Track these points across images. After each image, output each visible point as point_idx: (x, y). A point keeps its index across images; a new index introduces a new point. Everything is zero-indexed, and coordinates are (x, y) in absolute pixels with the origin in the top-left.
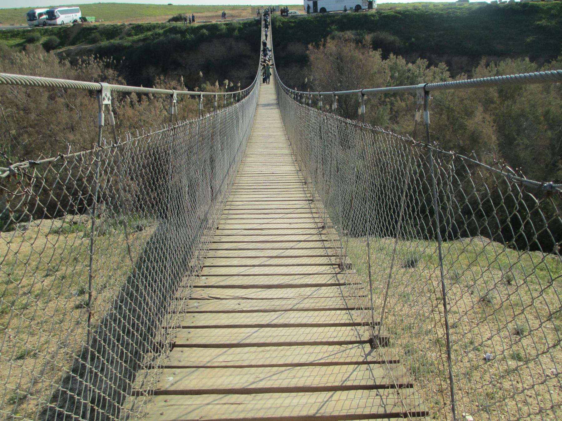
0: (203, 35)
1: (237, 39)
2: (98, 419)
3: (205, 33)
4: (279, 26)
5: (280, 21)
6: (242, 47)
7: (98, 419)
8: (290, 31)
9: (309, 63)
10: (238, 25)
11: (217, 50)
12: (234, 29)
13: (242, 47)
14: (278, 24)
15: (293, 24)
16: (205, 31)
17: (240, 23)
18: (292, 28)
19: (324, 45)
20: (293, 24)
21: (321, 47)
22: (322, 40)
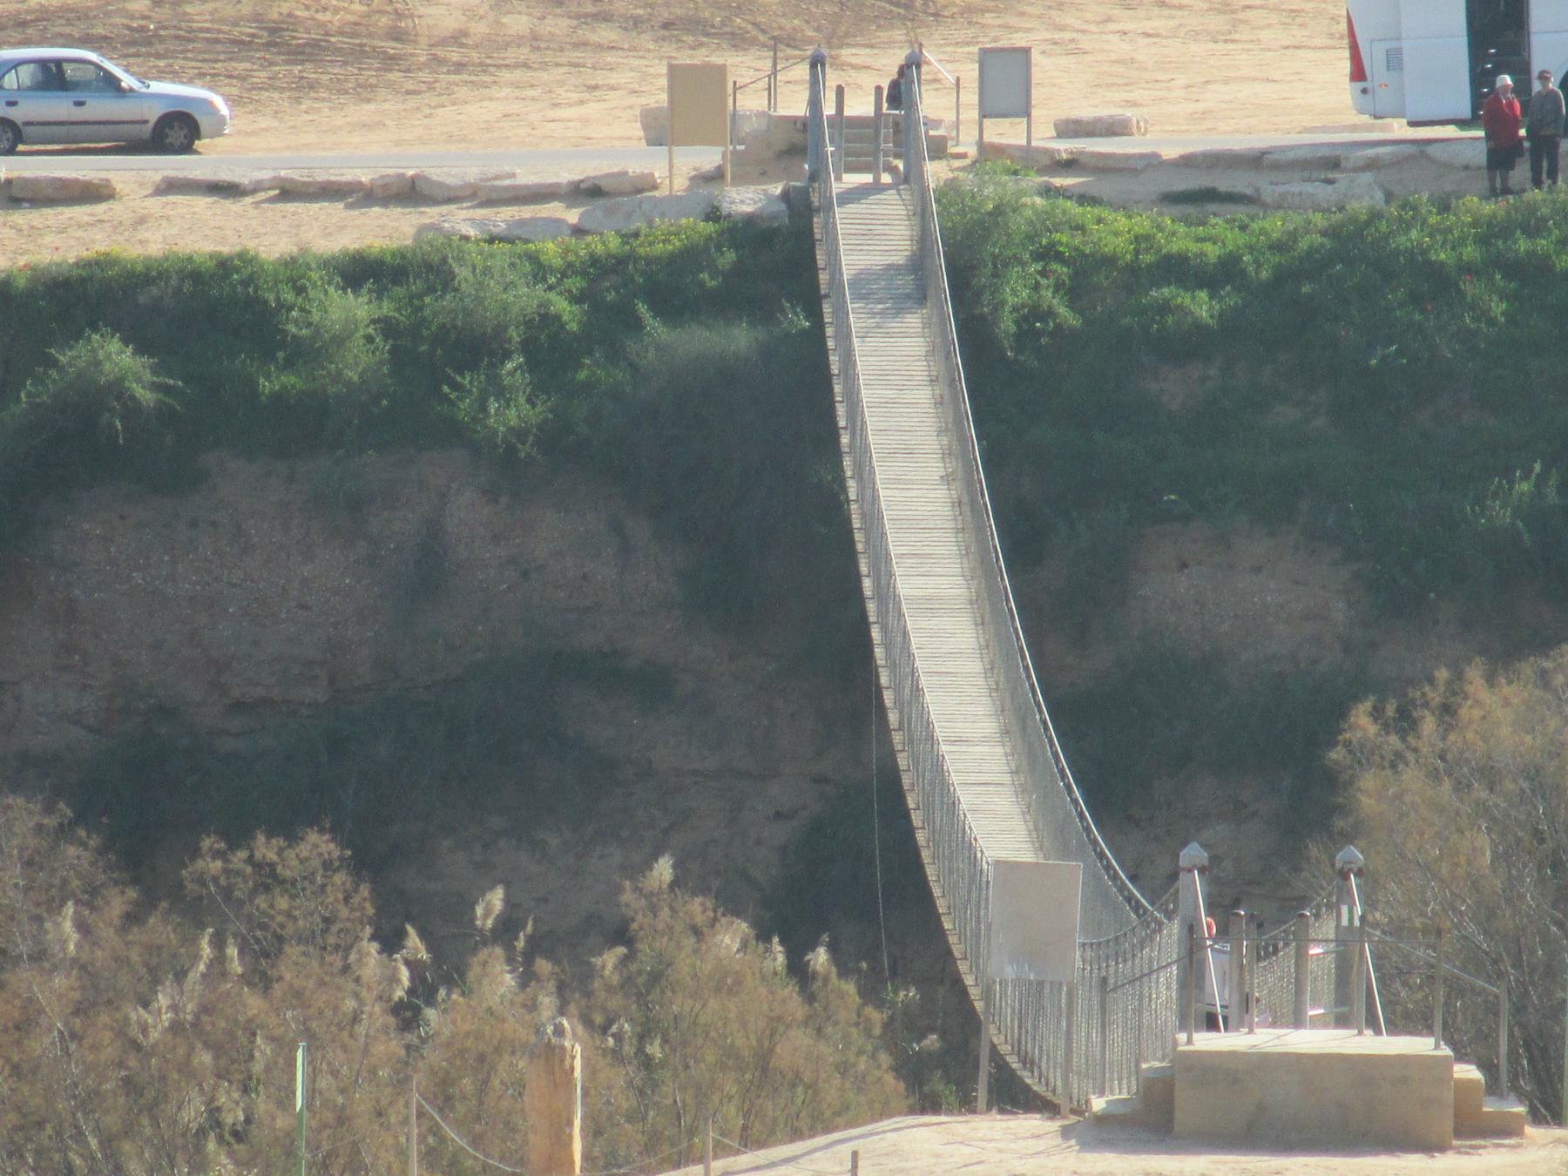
0: (92, 400)
1: (509, 470)
2: (14, 196)
3: (116, 389)
4: (1033, 314)
5: (1048, 254)
6: (576, 565)
7: (14, 196)
8: (1174, 389)
9: (1339, 823)
10: (526, 297)
11: (250, 589)
12: (473, 347)
13: (576, 565)
14: (1015, 292)
15: (1201, 306)
16: (117, 357)
17: (539, 271)
18: (1192, 345)
19: (1447, 711)
20: (1201, 306)
21: (1429, 725)
22: (1442, 674)
